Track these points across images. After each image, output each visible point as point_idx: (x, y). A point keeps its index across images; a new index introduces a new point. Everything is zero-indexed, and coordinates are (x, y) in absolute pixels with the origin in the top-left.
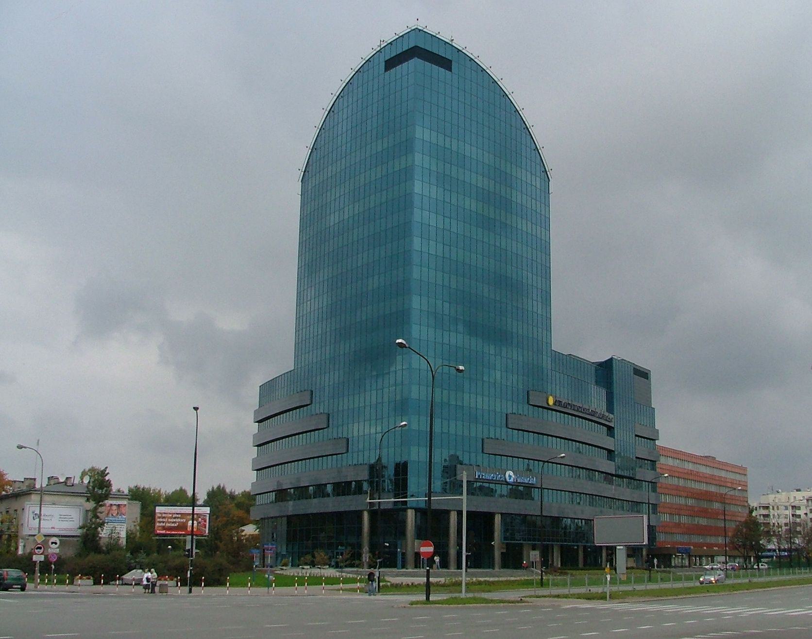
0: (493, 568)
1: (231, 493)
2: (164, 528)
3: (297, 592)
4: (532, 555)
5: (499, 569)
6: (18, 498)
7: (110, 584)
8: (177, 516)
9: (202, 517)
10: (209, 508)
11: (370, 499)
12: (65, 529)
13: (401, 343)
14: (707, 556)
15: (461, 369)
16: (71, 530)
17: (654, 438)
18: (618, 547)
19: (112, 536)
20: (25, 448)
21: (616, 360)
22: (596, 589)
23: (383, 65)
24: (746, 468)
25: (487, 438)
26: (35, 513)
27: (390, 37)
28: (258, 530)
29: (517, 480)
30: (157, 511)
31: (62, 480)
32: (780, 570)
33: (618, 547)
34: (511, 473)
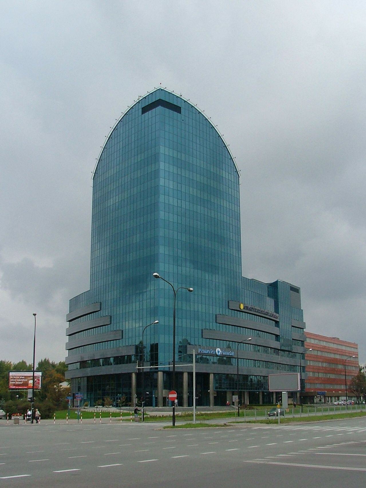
0: (209, 405)
2: (14, 385)
8: (22, 377)
11: (138, 367)
13: (156, 275)
14: (335, 397)
15: (191, 290)
18: (283, 392)
21: (280, 281)
27: (145, 94)
28: (69, 385)
30: (10, 375)
33: (283, 392)
34: (219, 349)
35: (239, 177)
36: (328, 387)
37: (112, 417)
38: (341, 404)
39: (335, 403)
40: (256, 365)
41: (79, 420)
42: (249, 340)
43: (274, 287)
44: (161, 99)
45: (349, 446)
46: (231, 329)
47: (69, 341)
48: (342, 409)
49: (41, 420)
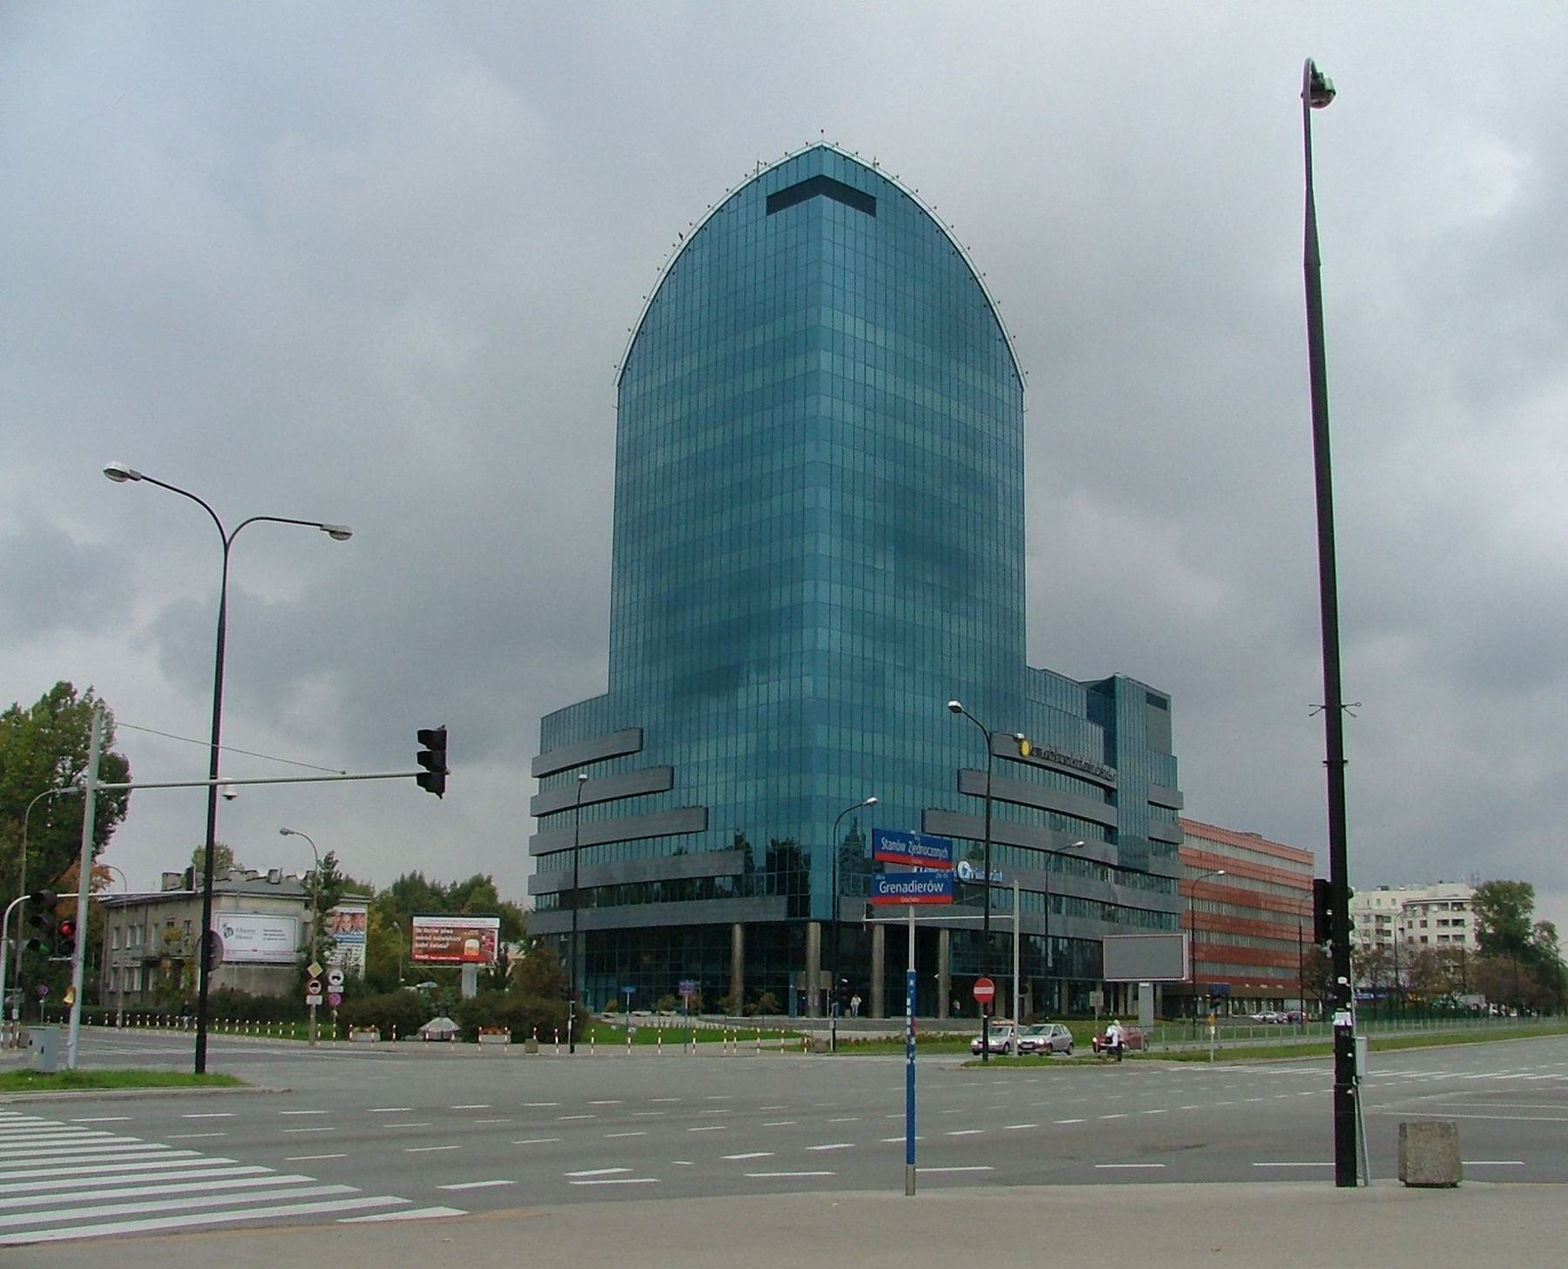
1: (433, 886)
2: (426, 951)
3: (631, 1052)
4: (1093, 997)
5: (947, 1017)
6: (191, 904)
7: (404, 1040)
8: (448, 932)
9: (487, 934)
10: (498, 920)
11: (867, 917)
12: (274, 953)
14: (1250, 1000)
16: (283, 953)
17: (1174, 806)
18: (1142, 985)
19: (346, 964)
20: (292, 833)
21: (1120, 679)
22: (1197, 1046)
23: (763, 204)
24: (1312, 853)
25: (930, 809)
26: (228, 926)
27: (776, 158)
28: (523, 952)
29: (975, 876)
30: (415, 924)
31: (263, 873)
32: (1431, 1022)
35: (1023, 390)
36: (1233, 971)
37: (737, 1040)
38: (1270, 1019)
39: (1254, 1016)
40: (1131, 919)
41: (688, 1045)
42: (1080, 846)
43: (1103, 695)
44: (822, 176)
45: (1467, 1096)
46: (972, 804)
47: (539, 831)
48: (1254, 1035)
49: (662, 1046)
